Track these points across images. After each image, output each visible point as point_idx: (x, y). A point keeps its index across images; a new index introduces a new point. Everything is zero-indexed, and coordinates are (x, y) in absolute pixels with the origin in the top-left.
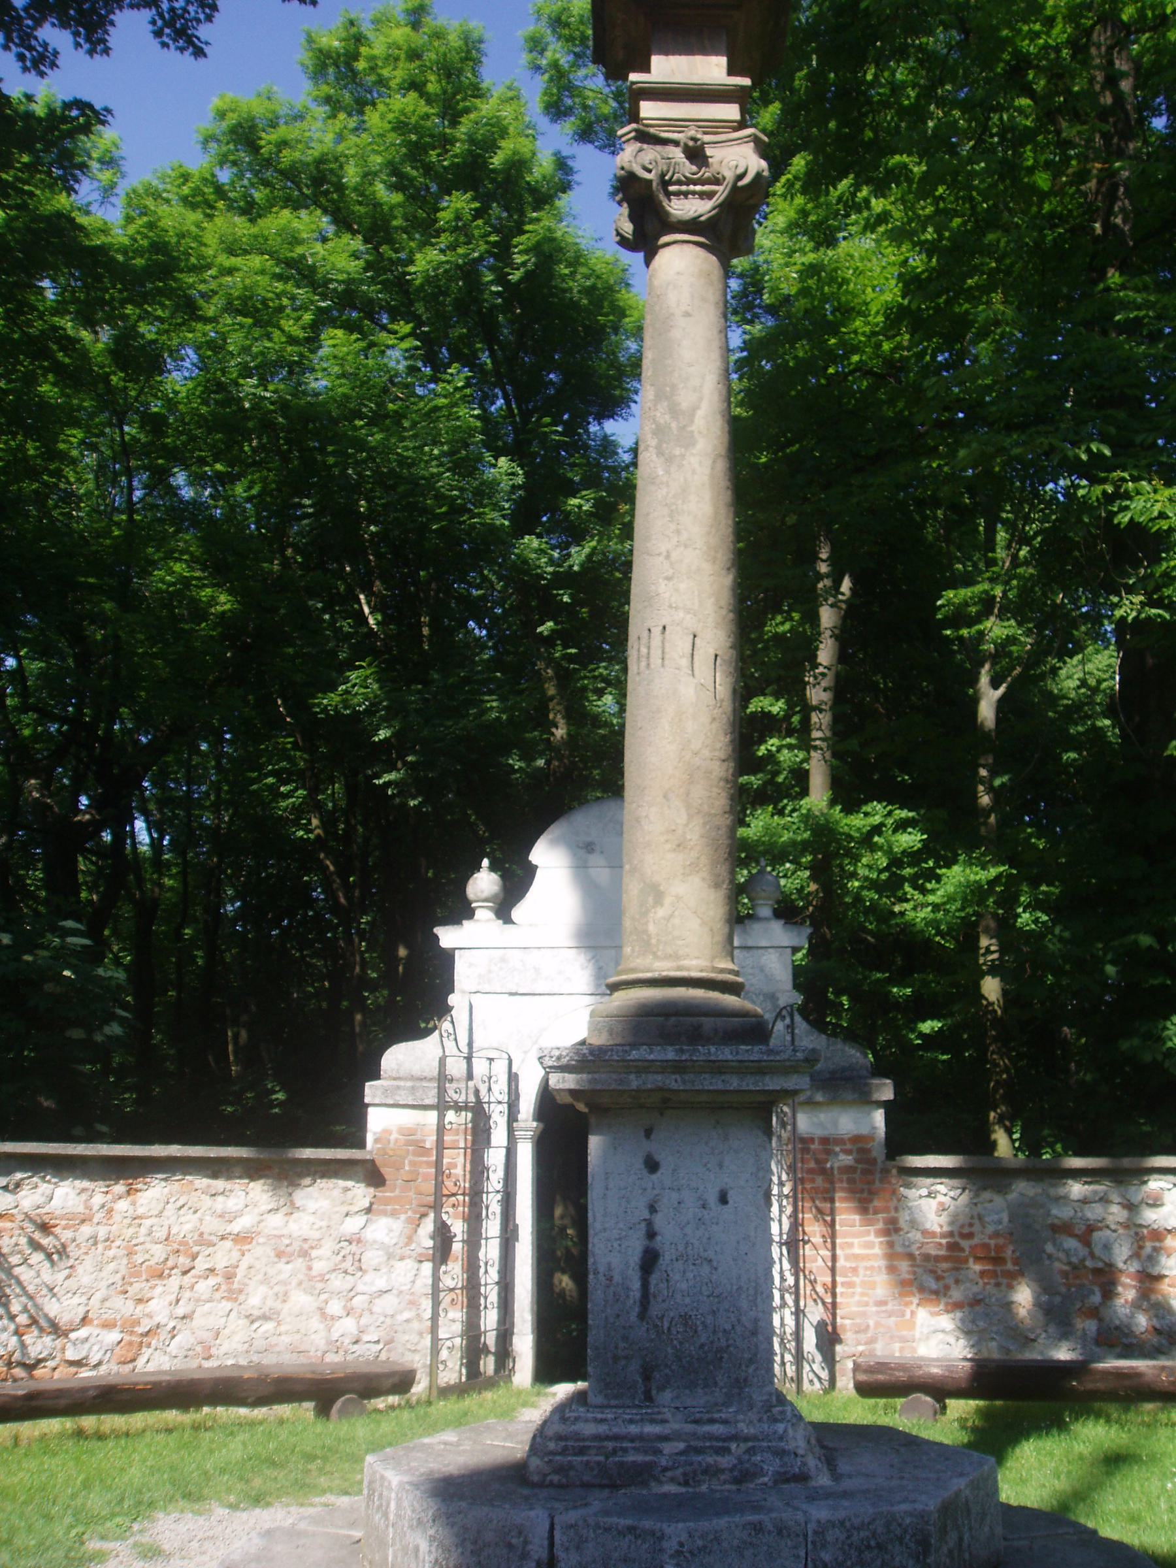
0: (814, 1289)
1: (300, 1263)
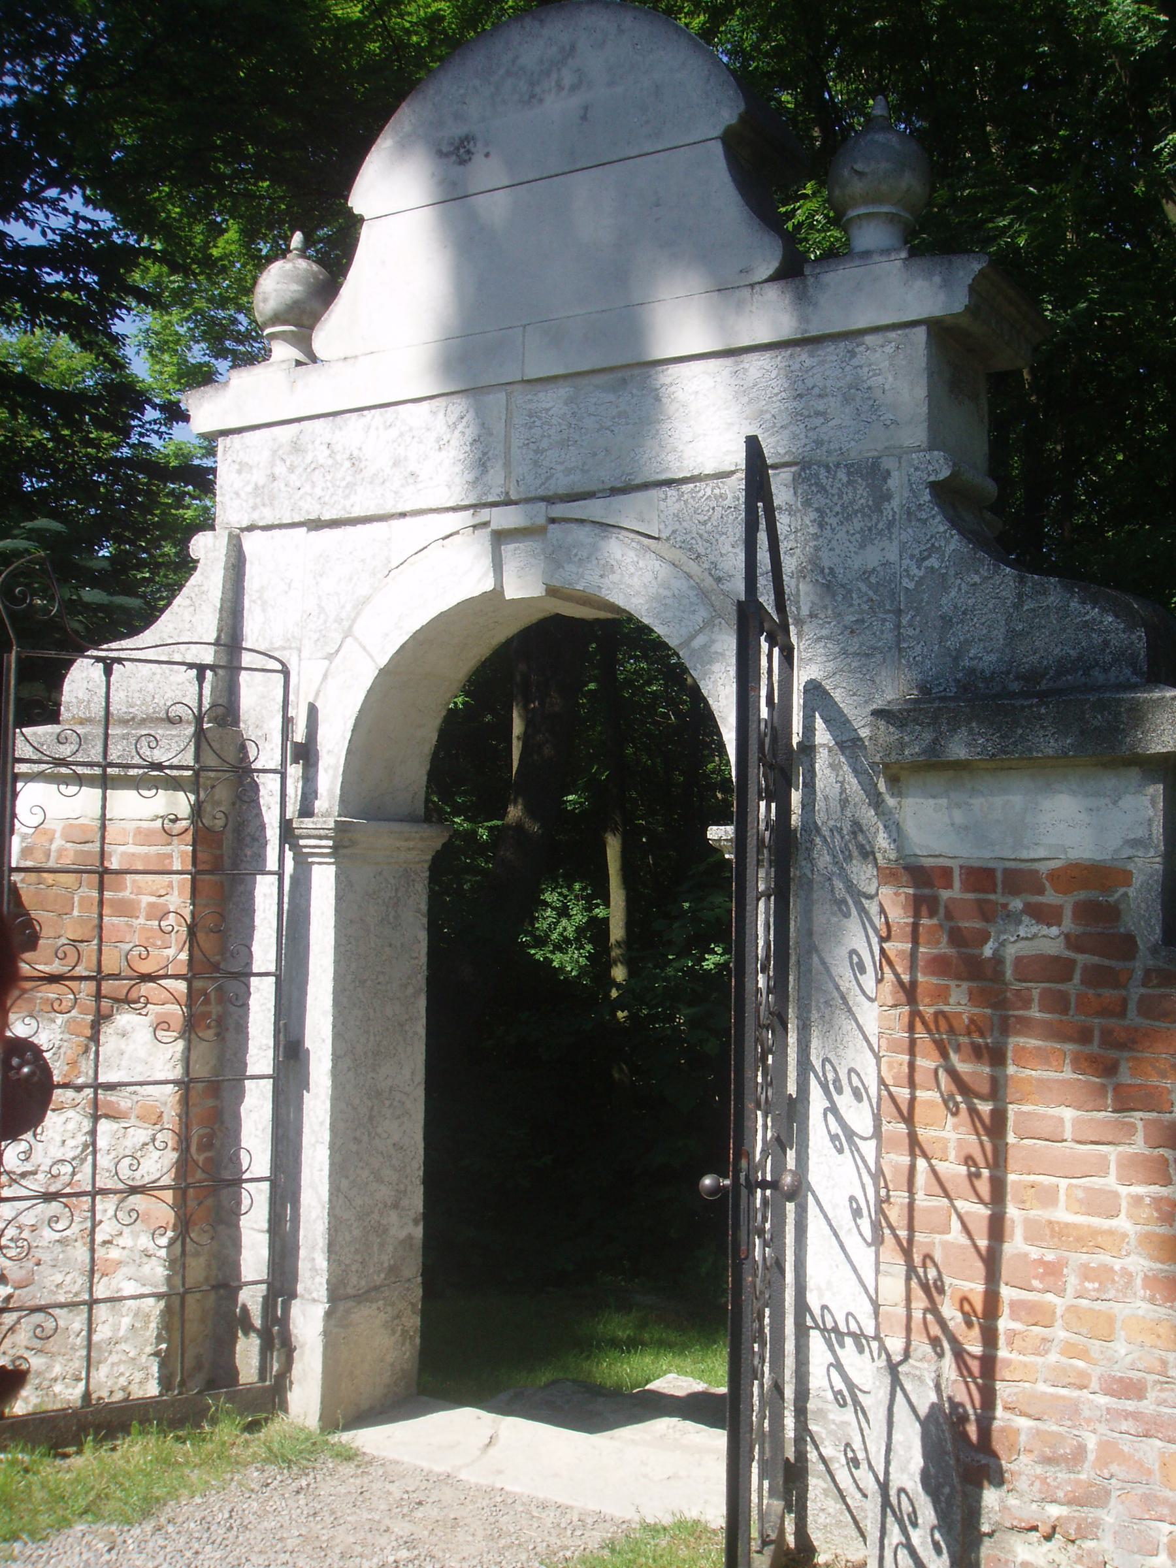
0: (933, 1309)
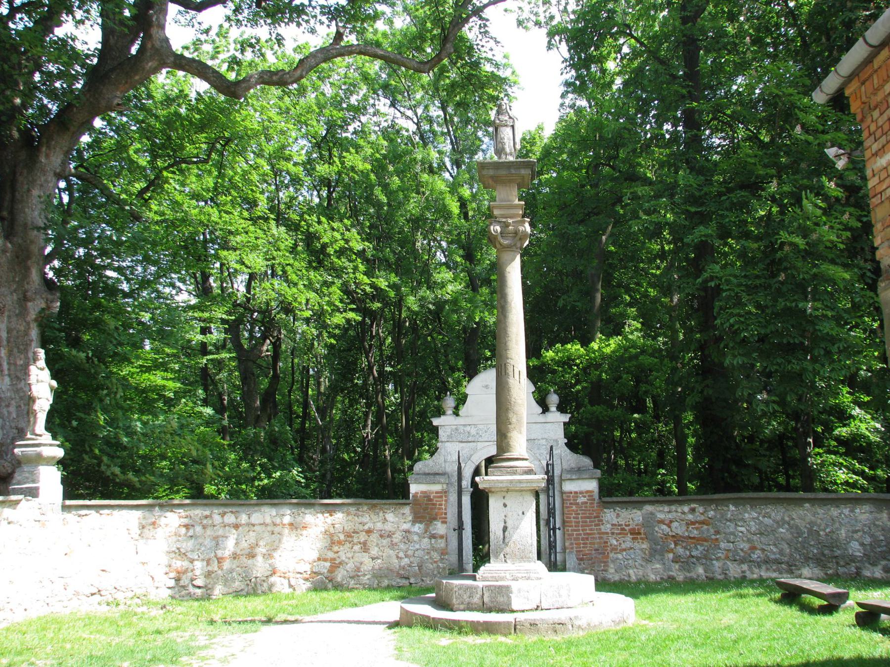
1: (389, 539)
